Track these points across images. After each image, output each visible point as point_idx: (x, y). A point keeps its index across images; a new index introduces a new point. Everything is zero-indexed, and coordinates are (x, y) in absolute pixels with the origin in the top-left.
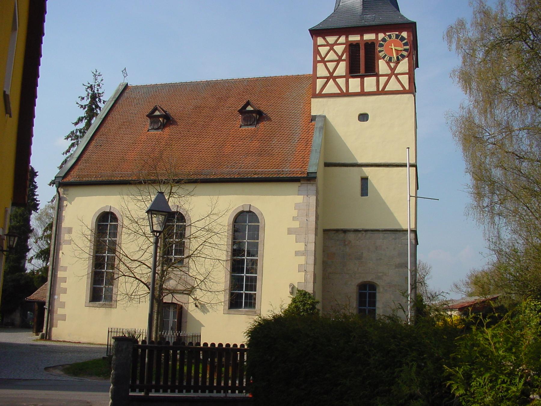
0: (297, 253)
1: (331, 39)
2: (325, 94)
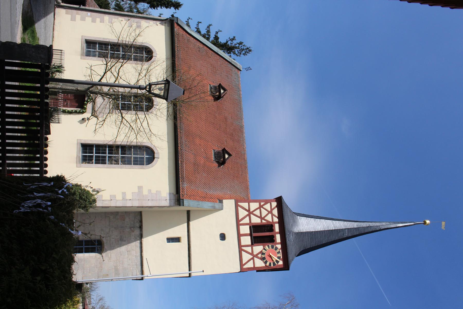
0: (124, 194)
1: (275, 212)
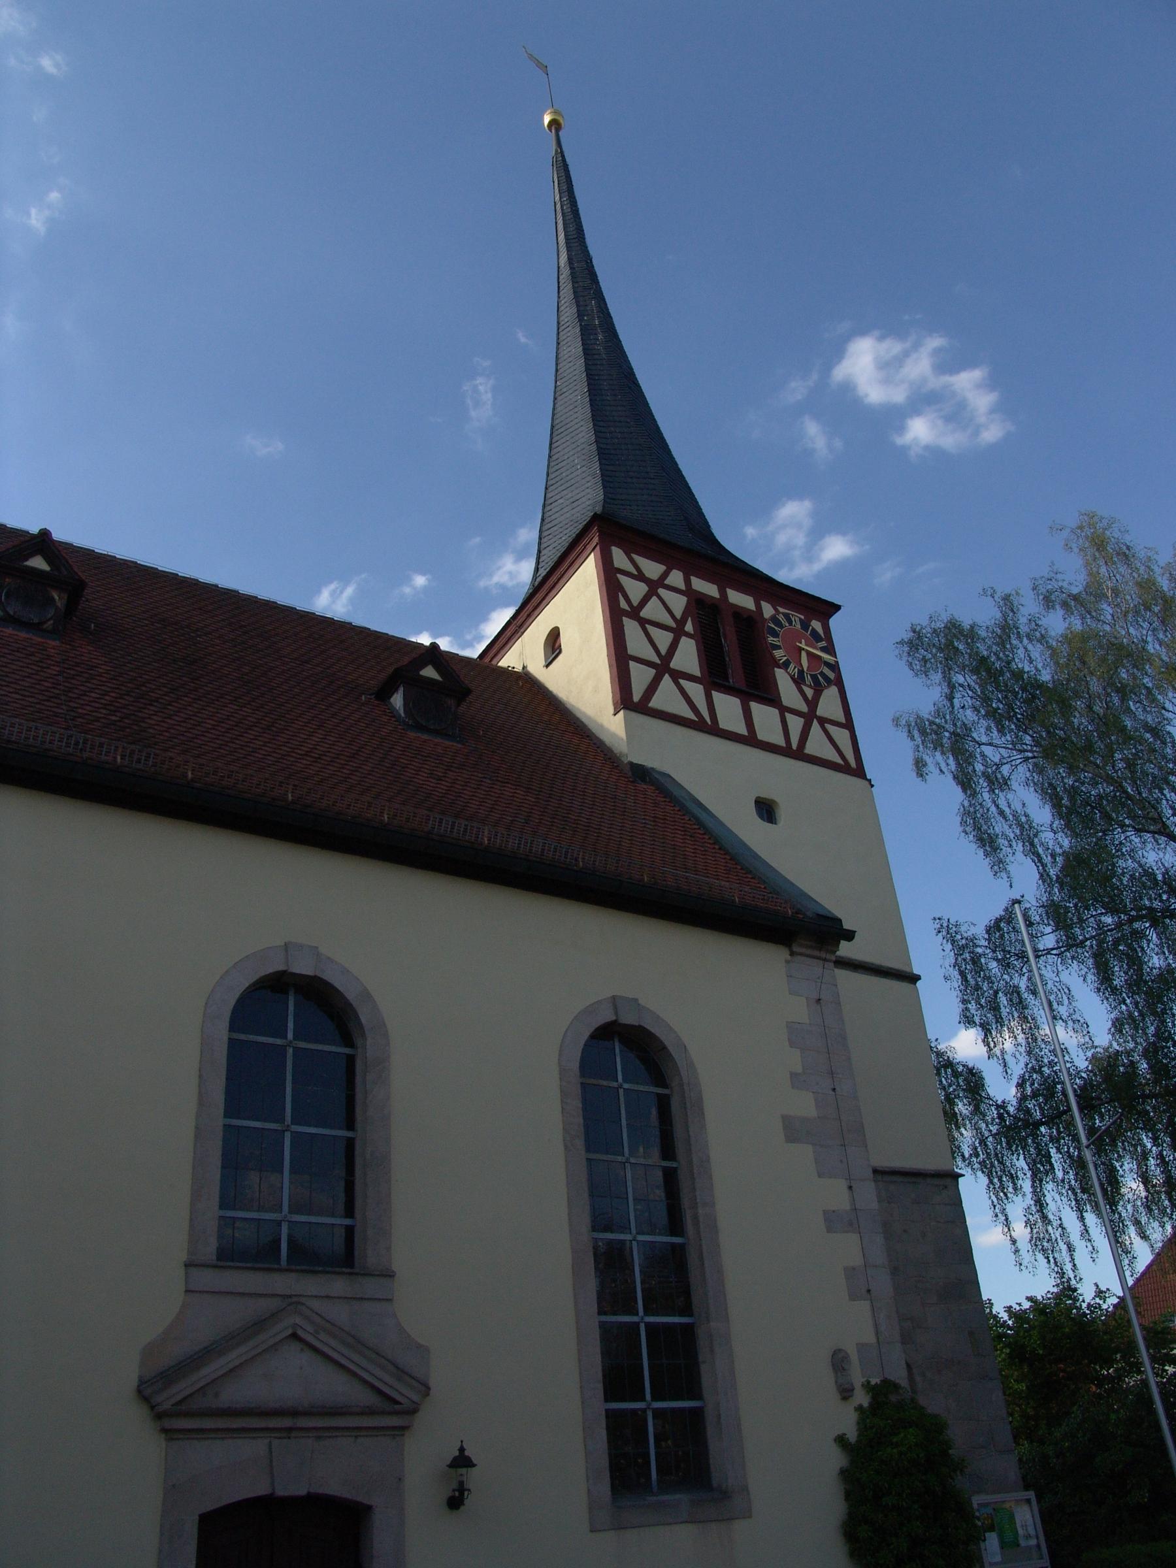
0: (832, 1221)
1: (653, 569)
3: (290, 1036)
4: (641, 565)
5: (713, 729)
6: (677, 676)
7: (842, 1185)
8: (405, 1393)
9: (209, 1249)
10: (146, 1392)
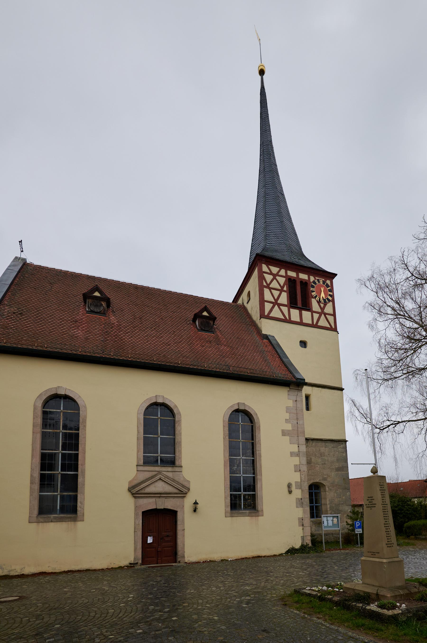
0: (292, 454)
1: (275, 270)
2: (272, 317)
3: (159, 416)
4: (271, 269)
5: (289, 321)
6: (279, 305)
7: (297, 446)
8: (185, 490)
9: (141, 462)
10: (130, 490)
